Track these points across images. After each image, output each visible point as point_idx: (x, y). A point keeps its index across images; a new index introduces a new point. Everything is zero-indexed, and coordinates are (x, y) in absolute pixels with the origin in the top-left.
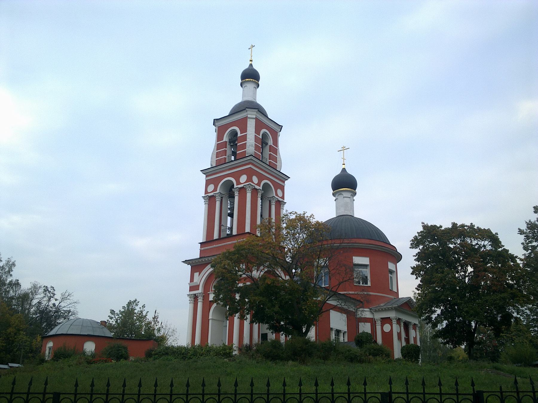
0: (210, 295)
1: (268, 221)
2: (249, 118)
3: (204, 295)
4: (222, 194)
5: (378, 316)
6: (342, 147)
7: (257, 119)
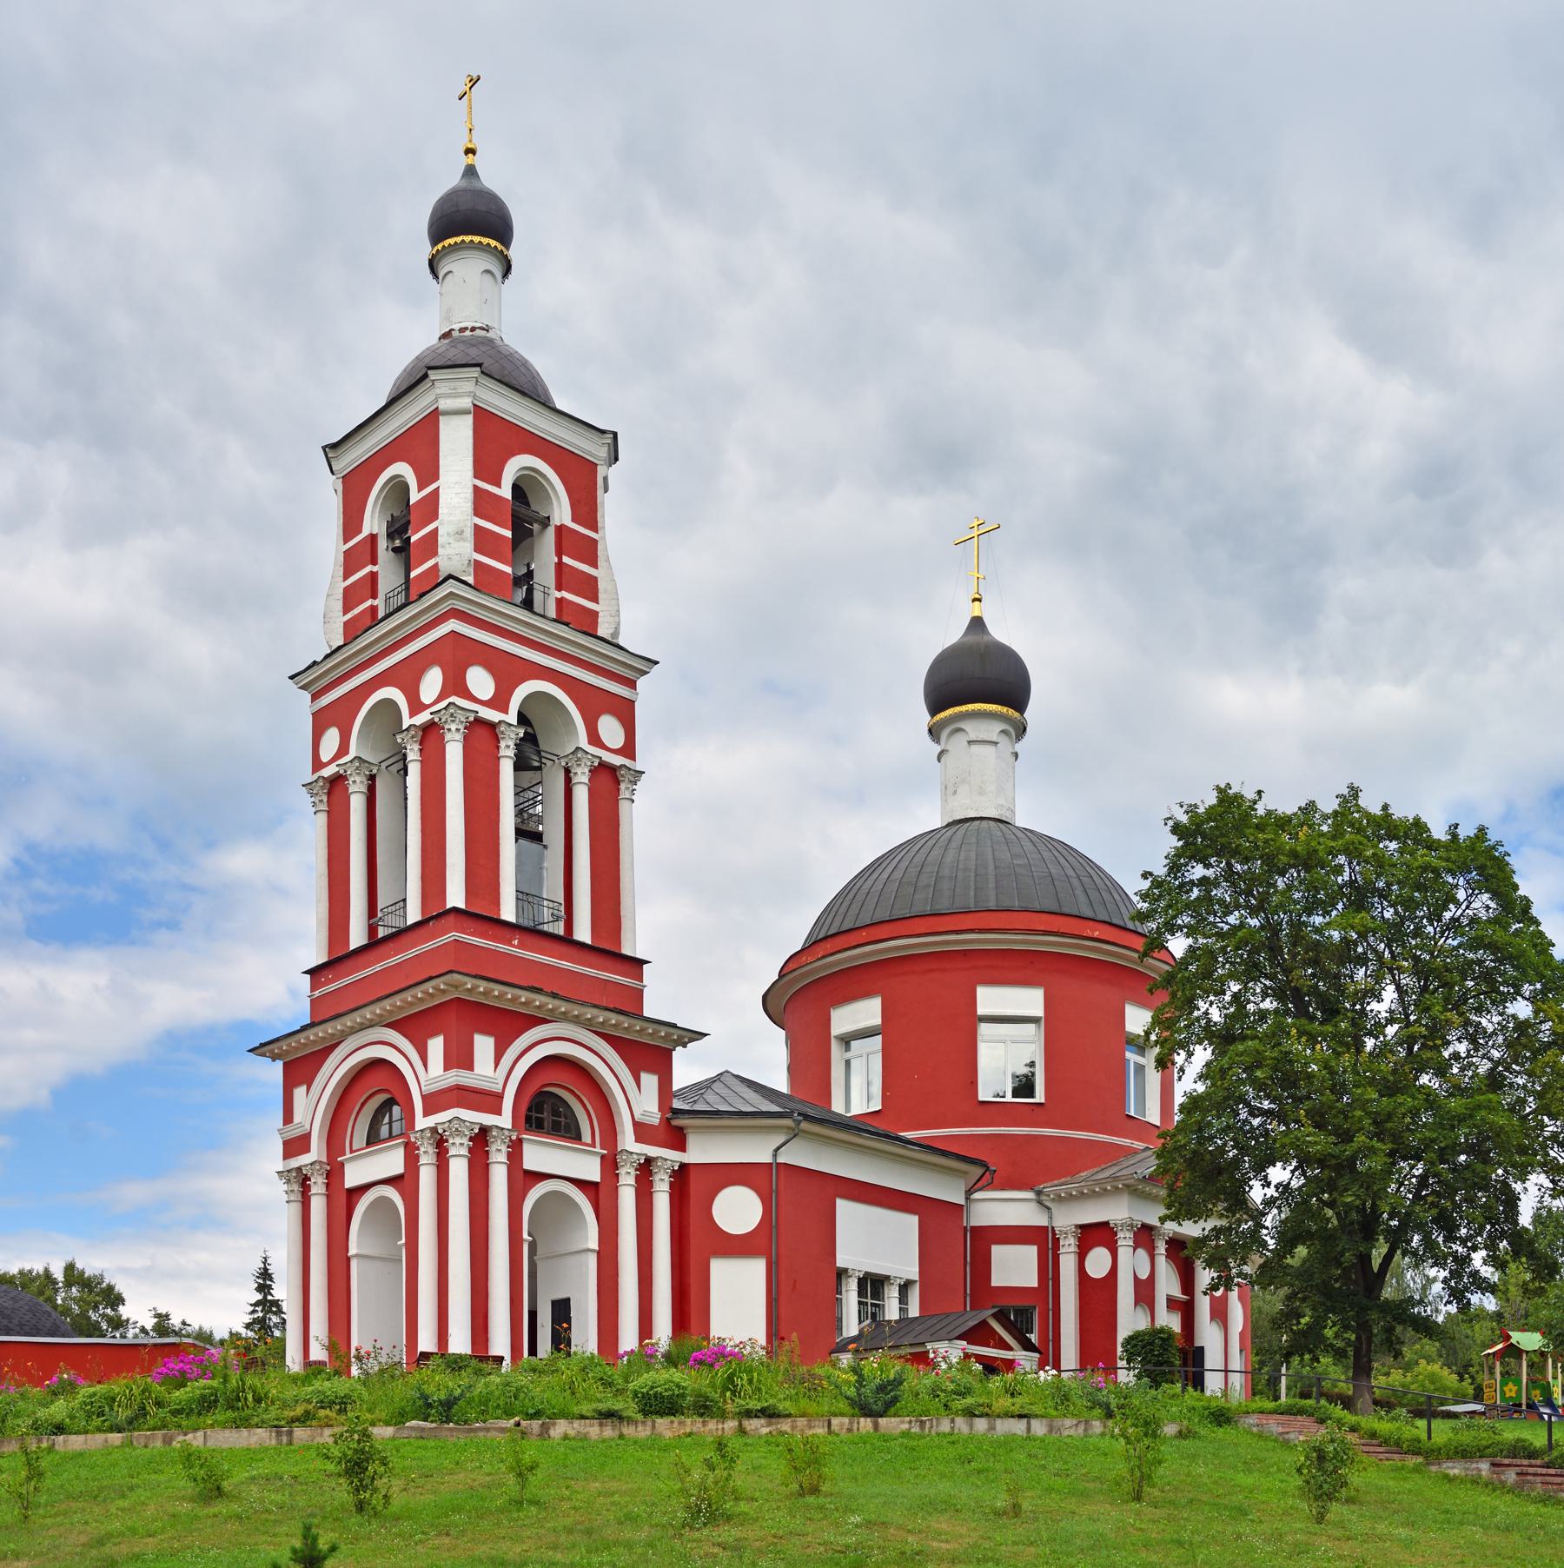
3: (328, 1168)
5: (1068, 1219)
7: (483, 418)
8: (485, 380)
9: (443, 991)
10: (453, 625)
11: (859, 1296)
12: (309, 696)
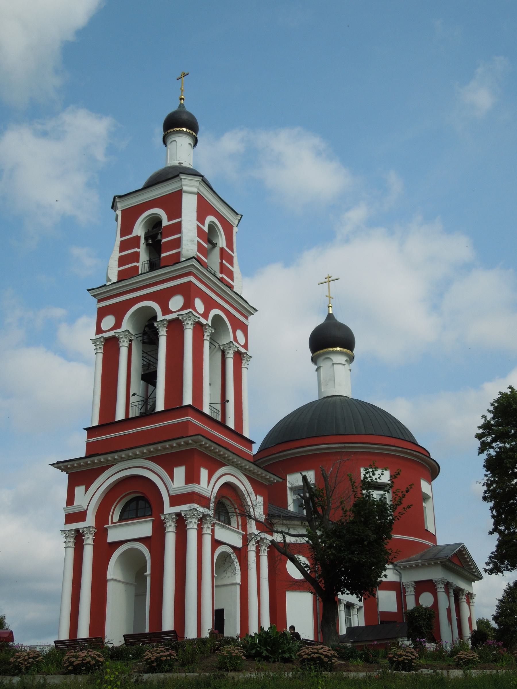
0: (109, 532)
2: (186, 192)
4: (131, 334)
6: (327, 276)
8: (202, 183)
12: (97, 300)
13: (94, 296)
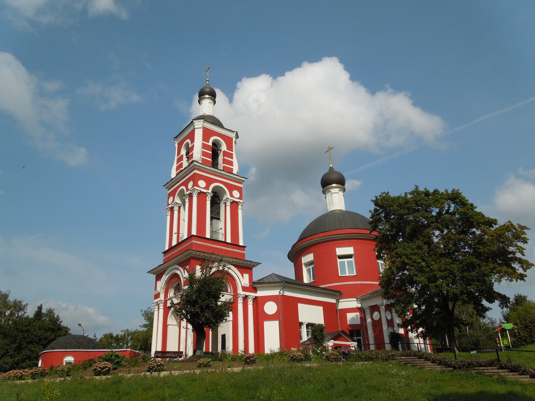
1: (477, 229)
6: (328, 148)
7: (205, 130)
9: (188, 255)
10: (196, 171)
11: (307, 329)
13: (166, 188)
